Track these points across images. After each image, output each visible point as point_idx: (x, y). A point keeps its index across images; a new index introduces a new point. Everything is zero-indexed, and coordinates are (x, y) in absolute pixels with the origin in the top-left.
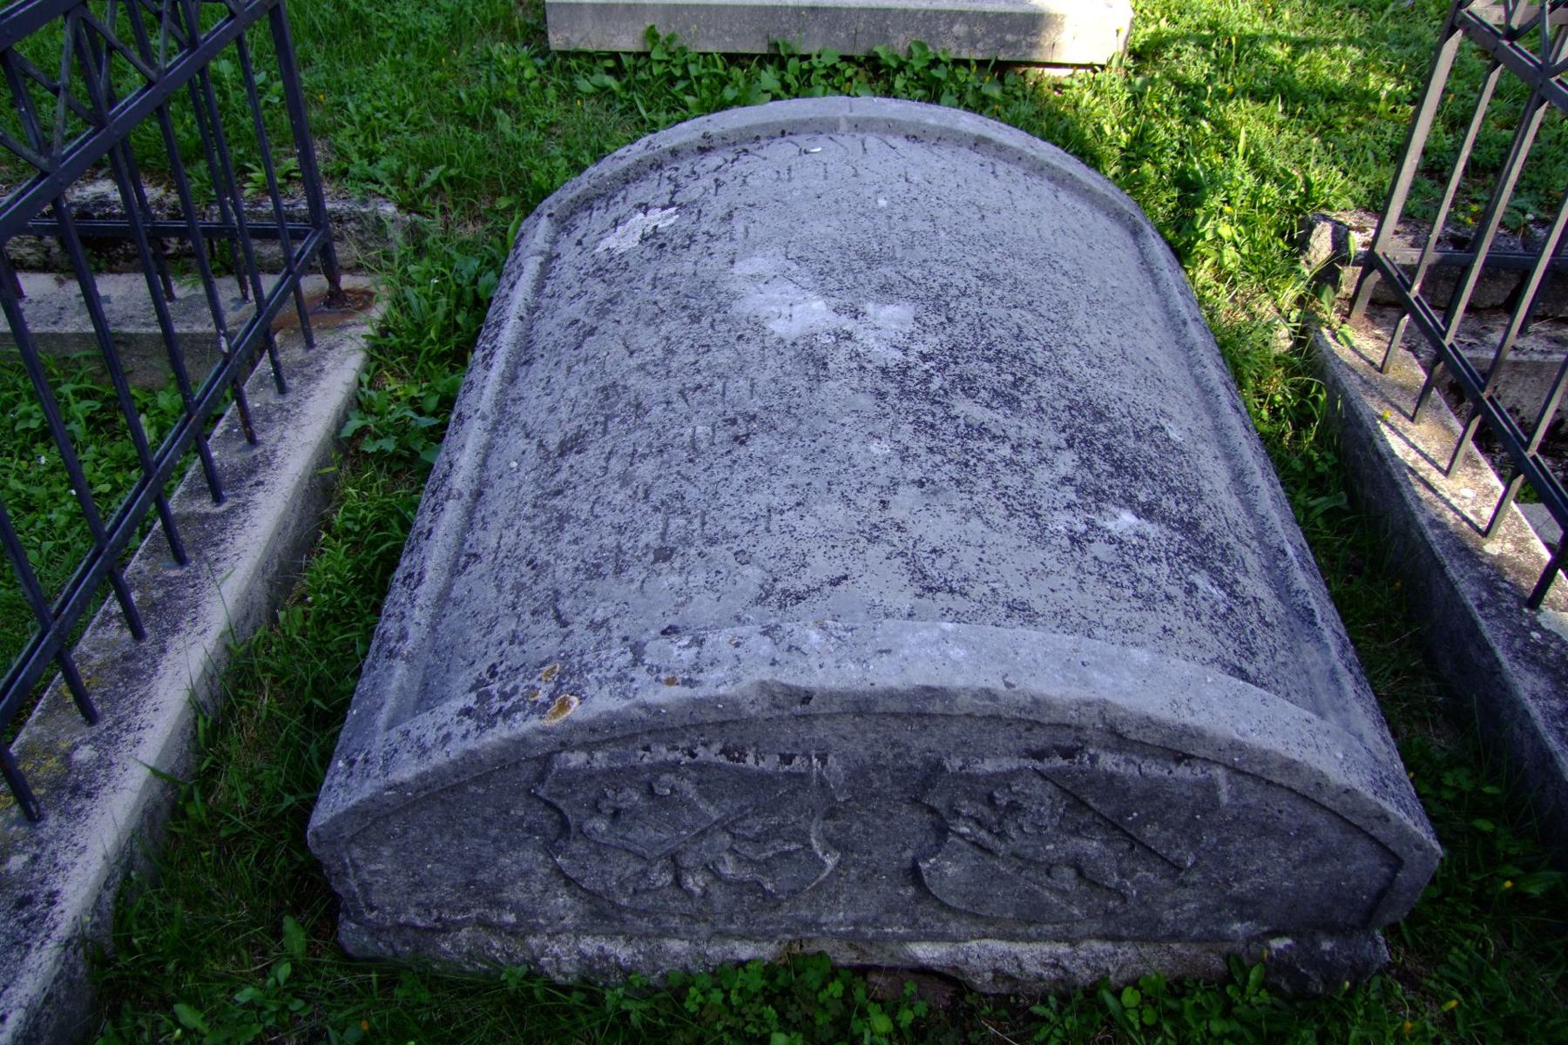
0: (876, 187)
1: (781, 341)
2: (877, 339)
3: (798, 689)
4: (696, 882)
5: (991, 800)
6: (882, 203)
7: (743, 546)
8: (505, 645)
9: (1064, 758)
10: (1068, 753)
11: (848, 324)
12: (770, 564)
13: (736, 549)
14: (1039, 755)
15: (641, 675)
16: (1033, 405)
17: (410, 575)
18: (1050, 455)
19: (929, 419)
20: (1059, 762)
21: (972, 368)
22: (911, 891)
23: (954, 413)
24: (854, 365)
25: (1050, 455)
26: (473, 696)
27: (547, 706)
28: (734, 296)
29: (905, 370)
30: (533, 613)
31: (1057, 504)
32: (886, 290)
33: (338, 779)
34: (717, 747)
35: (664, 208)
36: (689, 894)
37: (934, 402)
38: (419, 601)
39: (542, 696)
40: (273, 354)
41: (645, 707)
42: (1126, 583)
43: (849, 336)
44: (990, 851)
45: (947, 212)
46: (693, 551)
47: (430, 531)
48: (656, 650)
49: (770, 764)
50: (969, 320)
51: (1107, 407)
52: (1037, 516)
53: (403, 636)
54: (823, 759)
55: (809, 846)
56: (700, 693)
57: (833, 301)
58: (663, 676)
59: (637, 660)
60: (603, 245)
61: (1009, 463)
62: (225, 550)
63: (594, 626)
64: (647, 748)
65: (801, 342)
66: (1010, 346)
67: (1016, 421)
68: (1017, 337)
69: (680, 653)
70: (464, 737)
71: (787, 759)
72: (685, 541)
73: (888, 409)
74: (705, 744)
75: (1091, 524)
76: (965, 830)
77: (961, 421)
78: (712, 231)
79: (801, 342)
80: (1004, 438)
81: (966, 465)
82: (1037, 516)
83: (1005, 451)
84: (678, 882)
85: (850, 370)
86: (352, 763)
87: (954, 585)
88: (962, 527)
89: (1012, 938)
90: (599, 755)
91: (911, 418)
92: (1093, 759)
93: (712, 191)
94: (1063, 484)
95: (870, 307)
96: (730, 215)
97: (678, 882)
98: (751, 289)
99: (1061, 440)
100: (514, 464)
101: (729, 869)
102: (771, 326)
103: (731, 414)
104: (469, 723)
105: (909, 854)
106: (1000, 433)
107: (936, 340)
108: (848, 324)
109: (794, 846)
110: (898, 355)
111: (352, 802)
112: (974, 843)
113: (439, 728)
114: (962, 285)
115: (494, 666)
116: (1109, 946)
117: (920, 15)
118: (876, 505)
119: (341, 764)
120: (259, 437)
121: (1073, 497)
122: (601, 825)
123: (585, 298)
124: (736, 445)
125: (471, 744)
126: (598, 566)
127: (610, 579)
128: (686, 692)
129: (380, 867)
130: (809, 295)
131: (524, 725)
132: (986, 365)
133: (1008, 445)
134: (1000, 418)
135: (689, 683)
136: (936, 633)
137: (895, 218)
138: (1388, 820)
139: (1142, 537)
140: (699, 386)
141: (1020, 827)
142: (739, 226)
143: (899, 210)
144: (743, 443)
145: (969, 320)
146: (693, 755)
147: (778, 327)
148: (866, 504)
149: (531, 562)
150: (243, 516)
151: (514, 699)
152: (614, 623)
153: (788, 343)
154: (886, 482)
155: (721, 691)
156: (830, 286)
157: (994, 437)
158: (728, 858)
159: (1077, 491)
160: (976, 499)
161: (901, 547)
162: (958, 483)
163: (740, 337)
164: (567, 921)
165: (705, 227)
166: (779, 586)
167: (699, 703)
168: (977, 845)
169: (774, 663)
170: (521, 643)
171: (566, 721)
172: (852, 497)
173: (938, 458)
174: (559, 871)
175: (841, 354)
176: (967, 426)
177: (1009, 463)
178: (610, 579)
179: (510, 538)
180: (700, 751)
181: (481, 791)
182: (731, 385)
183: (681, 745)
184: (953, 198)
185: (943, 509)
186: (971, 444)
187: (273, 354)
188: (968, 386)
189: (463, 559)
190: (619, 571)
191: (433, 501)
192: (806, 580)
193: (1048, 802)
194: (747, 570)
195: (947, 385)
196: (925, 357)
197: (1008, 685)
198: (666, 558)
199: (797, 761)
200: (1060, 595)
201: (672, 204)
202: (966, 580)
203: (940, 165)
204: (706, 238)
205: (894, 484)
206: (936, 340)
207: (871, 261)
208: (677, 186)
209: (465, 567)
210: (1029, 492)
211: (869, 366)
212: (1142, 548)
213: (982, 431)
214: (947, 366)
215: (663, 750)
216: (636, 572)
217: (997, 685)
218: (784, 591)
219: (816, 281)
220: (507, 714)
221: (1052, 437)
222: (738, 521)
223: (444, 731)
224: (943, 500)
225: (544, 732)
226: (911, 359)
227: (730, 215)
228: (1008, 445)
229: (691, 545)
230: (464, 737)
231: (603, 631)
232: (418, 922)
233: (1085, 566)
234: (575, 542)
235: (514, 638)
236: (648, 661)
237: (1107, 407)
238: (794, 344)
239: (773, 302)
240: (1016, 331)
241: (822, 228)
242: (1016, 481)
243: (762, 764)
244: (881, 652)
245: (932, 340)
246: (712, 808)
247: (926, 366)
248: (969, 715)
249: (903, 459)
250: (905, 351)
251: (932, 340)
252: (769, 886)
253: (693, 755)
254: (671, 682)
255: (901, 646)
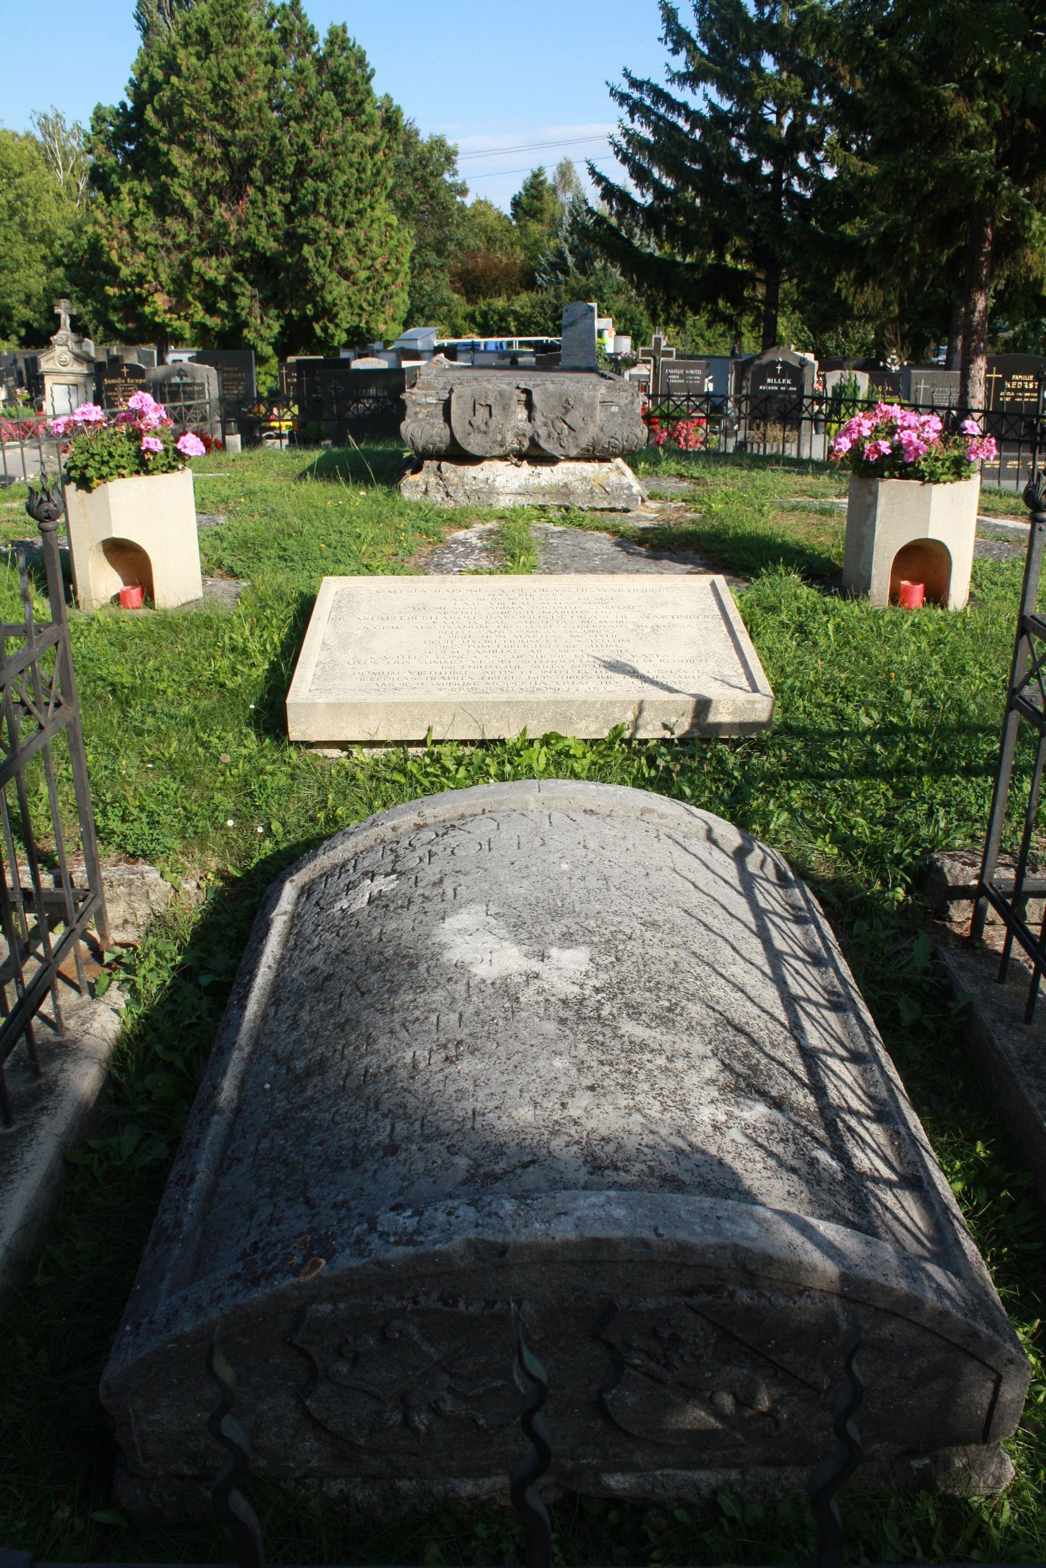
0: (560, 854)
1: (484, 981)
2: (559, 977)
3: (496, 1243)
4: (421, 1420)
5: (655, 1334)
6: (565, 867)
7: (454, 1141)
8: (264, 1225)
9: (709, 1294)
10: (710, 1290)
11: (535, 966)
12: (473, 1154)
13: (448, 1143)
14: (690, 1293)
15: (374, 1239)
16: (685, 1024)
17: (183, 1177)
18: (698, 1063)
19: (600, 1038)
20: (704, 1298)
21: (637, 997)
22: (600, 1422)
23: (620, 1033)
24: (541, 998)
25: (698, 1063)
26: (241, 1264)
27: (301, 1266)
28: (443, 946)
29: (582, 1001)
30: (288, 1200)
31: (703, 1100)
32: (568, 939)
33: (125, 1340)
34: (435, 1296)
35: (387, 875)
36: (416, 1431)
37: (604, 1025)
38: (193, 1196)
39: (297, 1260)
40: (55, 998)
41: (379, 1263)
42: (757, 1158)
43: (537, 976)
44: (660, 1381)
45: (618, 871)
46: (414, 1147)
47: (198, 1141)
48: (387, 1220)
49: (475, 1309)
50: (634, 959)
51: (747, 1023)
52: (685, 1110)
53: (179, 1224)
54: (519, 1303)
55: (513, 1381)
56: (421, 1250)
57: (525, 948)
58: (392, 1239)
59: (372, 1229)
60: (338, 906)
61: (664, 1070)
62: (16, 1164)
63: (335, 1206)
64: (380, 1299)
65: (498, 981)
66: (667, 978)
67: (670, 1038)
68: (672, 971)
69: (406, 1220)
70: (235, 1295)
71: (490, 1304)
72: (409, 1139)
73: (568, 1032)
74: (426, 1294)
75: (730, 1115)
76: (637, 1361)
77: (626, 1039)
78: (427, 894)
79: (498, 981)
80: (661, 1051)
81: (630, 1073)
82: (685, 1110)
83: (661, 1061)
84: (406, 1421)
85: (537, 1003)
86: (138, 1326)
87: (619, 1164)
88: (625, 1121)
89: (688, 1466)
90: (342, 1306)
91: (586, 1039)
92: (732, 1294)
93: (426, 860)
94: (707, 1084)
95: (554, 952)
96: (441, 880)
97: (406, 1421)
98: (459, 940)
99: (707, 1050)
100: (267, 1086)
101: (448, 1406)
102: (474, 970)
103: (443, 1040)
104: (238, 1284)
105: (594, 1387)
106: (657, 1047)
107: (606, 977)
108: (535, 966)
109: (500, 1383)
110: (576, 989)
111: (141, 1355)
112: (646, 1374)
113: (213, 1291)
114: (628, 931)
115: (256, 1243)
116: (772, 1472)
117: (598, 705)
118: (557, 1106)
119: (128, 1328)
120: (42, 1070)
121: (716, 1094)
122: (344, 1368)
123: (322, 950)
124: (447, 1064)
125: (241, 1300)
126: (339, 1161)
127: (349, 1171)
128: (410, 1250)
129: (158, 1416)
130: (506, 944)
131: (286, 1283)
132: (648, 994)
133: (664, 1057)
134: (659, 1036)
135: (411, 1242)
136: (603, 1198)
137: (575, 878)
138: (979, 1337)
139: (773, 1123)
140: (417, 1019)
141: (682, 1358)
142: (448, 886)
143: (578, 872)
144: (452, 1062)
145: (634, 959)
146: (416, 1303)
147: (482, 971)
148: (550, 1105)
149: (284, 1161)
150: (31, 1136)
151: (275, 1263)
152: (353, 1204)
153: (489, 982)
154: (566, 1089)
155: (437, 1247)
156: (522, 936)
157: (652, 1051)
158: (448, 1397)
159: (719, 1090)
160: (637, 1098)
161: (577, 1138)
162: (623, 1086)
163: (450, 979)
164: (314, 1464)
165: (421, 891)
166: (481, 1171)
167: (419, 1258)
168: (649, 1375)
169: (477, 1225)
170: (277, 1225)
171: (318, 1277)
172: (539, 1100)
173: (607, 1069)
174: (307, 1414)
175: (530, 991)
176: (631, 1042)
177: (664, 1070)
178: (349, 1171)
179: (265, 1144)
180: (422, 1299)
181: (246, 1342)
182: (443, 1019)
183: (408, 1294)
184: (622, 860)
185: (611, 1107)
186: (636, 1057)
187: (55, 998)
188: (634, 1011)
189: (226, 1164)
190: (355, 1165)
191: (199, 1117)
192: (502, 1164)
193: (701, 1333)
194: (456, 1159)
195: (615, 1011)
196: (597, 990)
197: (659, 1235)
198: (394, 1154)
199: (498, 1306)
200: (703, 1170)
201: (394, 871)
202: (628, 1160)
203: (612, 833)
204: (421, 899)
205: (572, 1091)
206: (606, 977)
207: (556, 914)
208: (397, 856)
209: (228, 1169)
210: (679, 1092)
211: (553, 999)
212: (772, 1132)
213: (643, 1046)
214: (615, 996)
215: (393, 1299)
216: (371, 1165)
217: (648, 1234)
218: (486, 1174)
219: (510, 932)
220: (269, 1276)
221: (699, 1048)
222: (449, 1123)
223: (218, 1292)
224: (610, 1100)
225: (297, 1287)
226: (587, 992)
227: (441, 880)
228: (664, 1057)
229: (412, 1142)
230: (235, 1295)
231: (343, 1212)
232: (187, 1471)
233: (725, 1147)
234: (321, 1144)
235: (273, 1221)
236: (380, 1229)
237: (747, 1023)
238: (493, 984)
239: (476, 951)
240: (672, 965)
241: (518, 890)
242: (671, 1084)
243: (471, 1309)
244: (559, 1214)
245: (603, 976)
246: (432, 1350)
247: (599, 997)
248: (630, 1261)
249: (579, 1070)
250: (582, 986)
251: (603, 976)
252: (481, 1422)
253: (416, 1303)
254: (397, 1243)
255: (576, 1209)
